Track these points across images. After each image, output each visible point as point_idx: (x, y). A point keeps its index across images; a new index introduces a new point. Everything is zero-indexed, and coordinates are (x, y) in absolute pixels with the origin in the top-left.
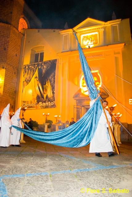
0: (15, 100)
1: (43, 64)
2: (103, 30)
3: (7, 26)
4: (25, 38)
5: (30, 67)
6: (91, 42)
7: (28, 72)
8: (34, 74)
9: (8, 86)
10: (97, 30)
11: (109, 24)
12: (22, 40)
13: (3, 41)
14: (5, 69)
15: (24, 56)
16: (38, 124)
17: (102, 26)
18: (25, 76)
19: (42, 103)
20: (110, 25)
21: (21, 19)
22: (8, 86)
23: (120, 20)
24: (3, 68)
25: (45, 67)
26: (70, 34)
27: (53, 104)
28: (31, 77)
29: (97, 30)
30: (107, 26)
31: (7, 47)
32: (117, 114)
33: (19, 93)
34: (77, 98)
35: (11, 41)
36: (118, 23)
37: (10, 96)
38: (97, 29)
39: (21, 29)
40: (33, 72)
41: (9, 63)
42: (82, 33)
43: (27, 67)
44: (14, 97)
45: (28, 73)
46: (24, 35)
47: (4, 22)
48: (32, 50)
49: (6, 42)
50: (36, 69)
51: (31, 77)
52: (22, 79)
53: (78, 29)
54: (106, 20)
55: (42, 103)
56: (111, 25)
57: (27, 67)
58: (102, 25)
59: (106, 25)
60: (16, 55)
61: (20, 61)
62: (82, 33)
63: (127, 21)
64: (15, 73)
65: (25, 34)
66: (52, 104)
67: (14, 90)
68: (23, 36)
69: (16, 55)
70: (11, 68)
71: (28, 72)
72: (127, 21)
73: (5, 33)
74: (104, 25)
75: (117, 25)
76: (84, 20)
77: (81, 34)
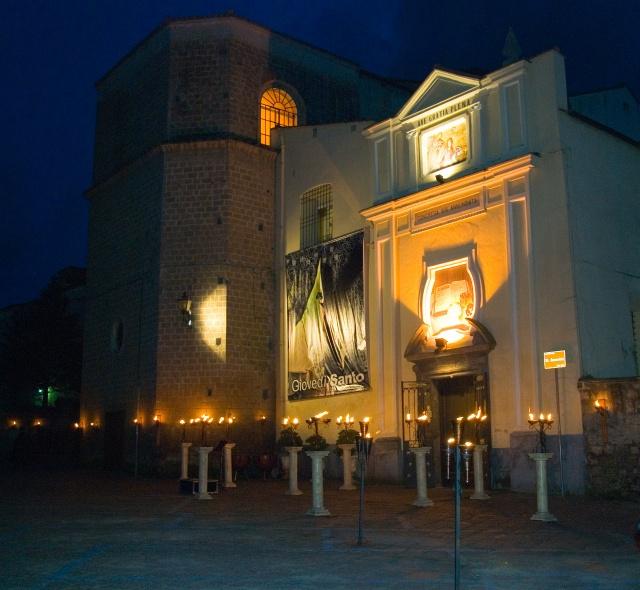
0: (274, 372)
1: (332, 249)
2: (477, 106)
3: (216, 146)
4: (283, 161)
5: (302, 259)
6: (451, 156)
7: (298, 278)
8: (312, 285)
9: (241, 334)
10: (464, 109)
11: (491, 83)
12: (275, 166)
13: (210, 198)
14: (227, 282)
15: (285, 225)
16: (327, 442)
17: (477, 92)
18: (292, 292)
19: (338, 376)
20: (495, 85)
21: (265, 95)
22: (241, 334)
23: (522, 63)
24: (220, 282)
25: (336, 257)
26: (394, 132)
27: (363, 378)
28: (306, 294)
29: (464, 109)
30: (490, 90)
31: (226, 214)
32: (185, 476)
33: (281, 348)
34: (415, 358)
35: (234, 190)
36: (520, 73)
37: (252, 363)
38: (464, 104)
39: (271, 129)
40: (310, 277)
41: (235, 261)
42: (424, 126)
43: (294, 262)
44: (269, 362)
45: (298, 282)
46: (278, 151)
47: (204, 138)
48: (305, 201)
49: (220, 200)
50: (317, 267)
51: (306, 294)
52: (287, 303)
53: (409, 113)
54: (478, 70)
55: (338, 376)
56: (501, 86)
57: (294, 262)
58: (475, 88)
59: (488, 88)
60: (261, 228)
61: (276, 241)
62: (424, 126)
63: (550, 65)
64: (263, 286)
65: (283, 147)
66: (360, 378)
67: (268, 342)
68: (276, 154)
69: (261, 228)
70: (246, 277)
71: (298, 278)
72: (550, 65)
73: (214, 171)
74: (481, 87)
75: (518, 82)
76: (444, 70)
77: (423, 130)
